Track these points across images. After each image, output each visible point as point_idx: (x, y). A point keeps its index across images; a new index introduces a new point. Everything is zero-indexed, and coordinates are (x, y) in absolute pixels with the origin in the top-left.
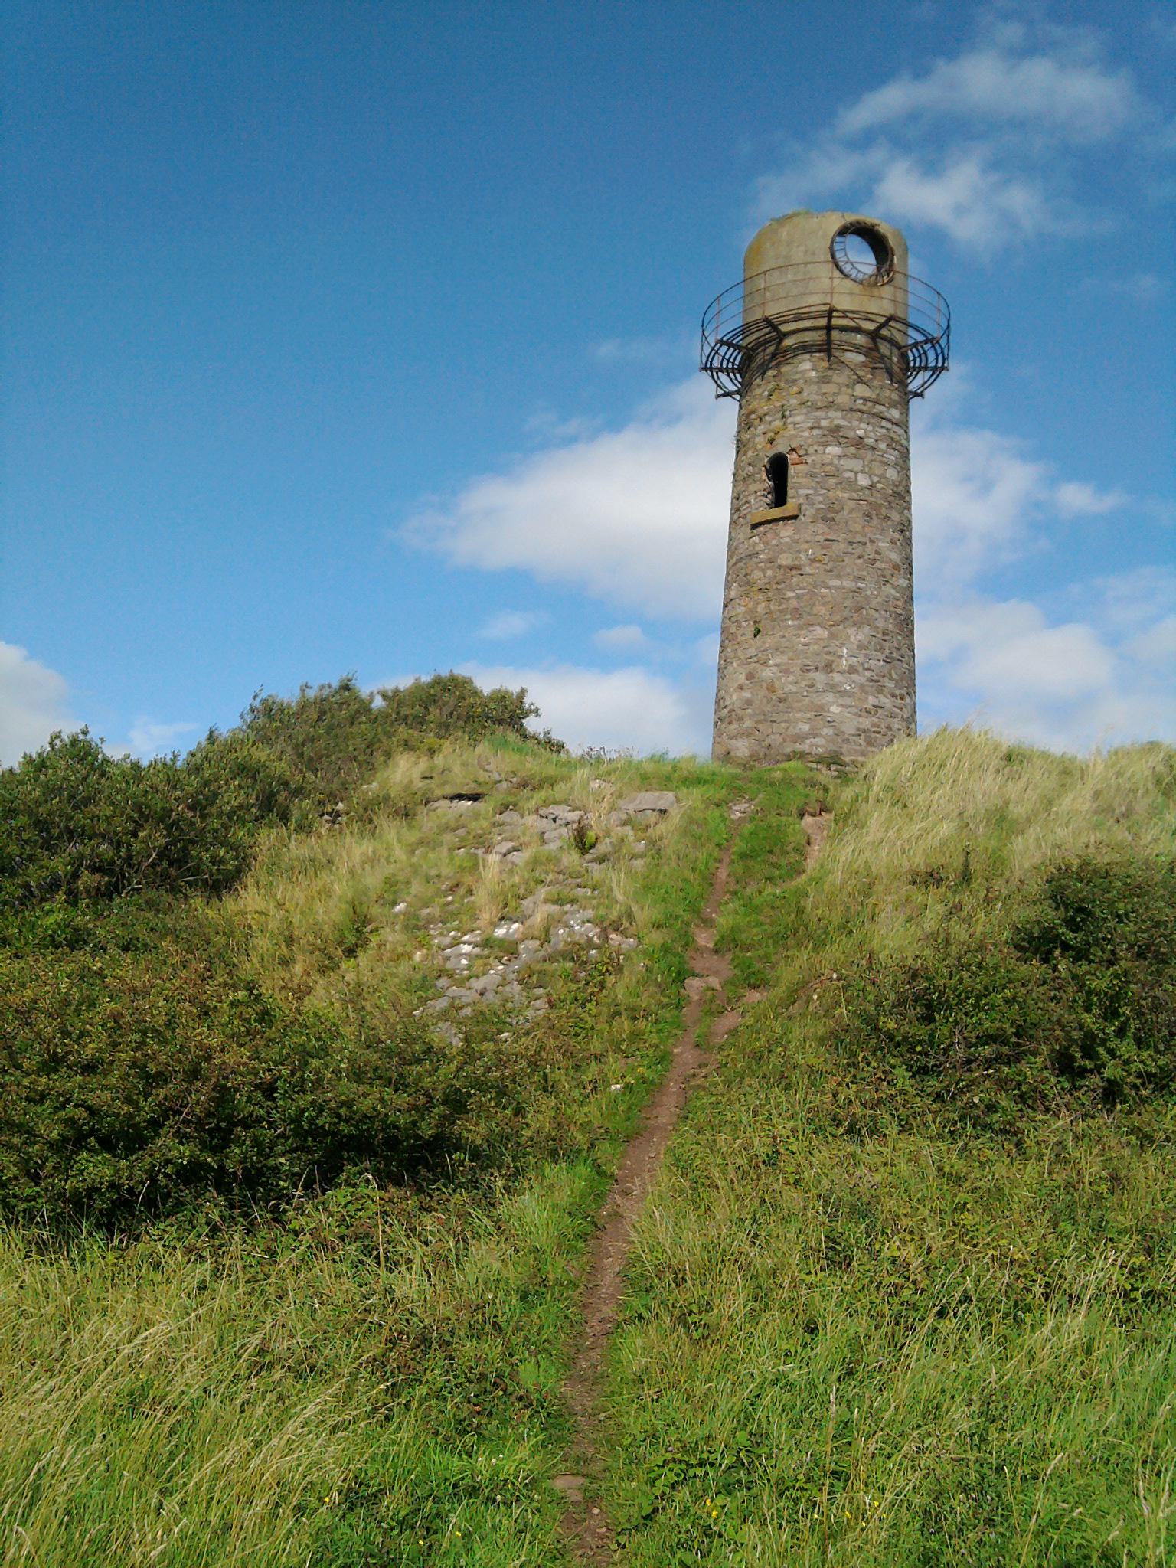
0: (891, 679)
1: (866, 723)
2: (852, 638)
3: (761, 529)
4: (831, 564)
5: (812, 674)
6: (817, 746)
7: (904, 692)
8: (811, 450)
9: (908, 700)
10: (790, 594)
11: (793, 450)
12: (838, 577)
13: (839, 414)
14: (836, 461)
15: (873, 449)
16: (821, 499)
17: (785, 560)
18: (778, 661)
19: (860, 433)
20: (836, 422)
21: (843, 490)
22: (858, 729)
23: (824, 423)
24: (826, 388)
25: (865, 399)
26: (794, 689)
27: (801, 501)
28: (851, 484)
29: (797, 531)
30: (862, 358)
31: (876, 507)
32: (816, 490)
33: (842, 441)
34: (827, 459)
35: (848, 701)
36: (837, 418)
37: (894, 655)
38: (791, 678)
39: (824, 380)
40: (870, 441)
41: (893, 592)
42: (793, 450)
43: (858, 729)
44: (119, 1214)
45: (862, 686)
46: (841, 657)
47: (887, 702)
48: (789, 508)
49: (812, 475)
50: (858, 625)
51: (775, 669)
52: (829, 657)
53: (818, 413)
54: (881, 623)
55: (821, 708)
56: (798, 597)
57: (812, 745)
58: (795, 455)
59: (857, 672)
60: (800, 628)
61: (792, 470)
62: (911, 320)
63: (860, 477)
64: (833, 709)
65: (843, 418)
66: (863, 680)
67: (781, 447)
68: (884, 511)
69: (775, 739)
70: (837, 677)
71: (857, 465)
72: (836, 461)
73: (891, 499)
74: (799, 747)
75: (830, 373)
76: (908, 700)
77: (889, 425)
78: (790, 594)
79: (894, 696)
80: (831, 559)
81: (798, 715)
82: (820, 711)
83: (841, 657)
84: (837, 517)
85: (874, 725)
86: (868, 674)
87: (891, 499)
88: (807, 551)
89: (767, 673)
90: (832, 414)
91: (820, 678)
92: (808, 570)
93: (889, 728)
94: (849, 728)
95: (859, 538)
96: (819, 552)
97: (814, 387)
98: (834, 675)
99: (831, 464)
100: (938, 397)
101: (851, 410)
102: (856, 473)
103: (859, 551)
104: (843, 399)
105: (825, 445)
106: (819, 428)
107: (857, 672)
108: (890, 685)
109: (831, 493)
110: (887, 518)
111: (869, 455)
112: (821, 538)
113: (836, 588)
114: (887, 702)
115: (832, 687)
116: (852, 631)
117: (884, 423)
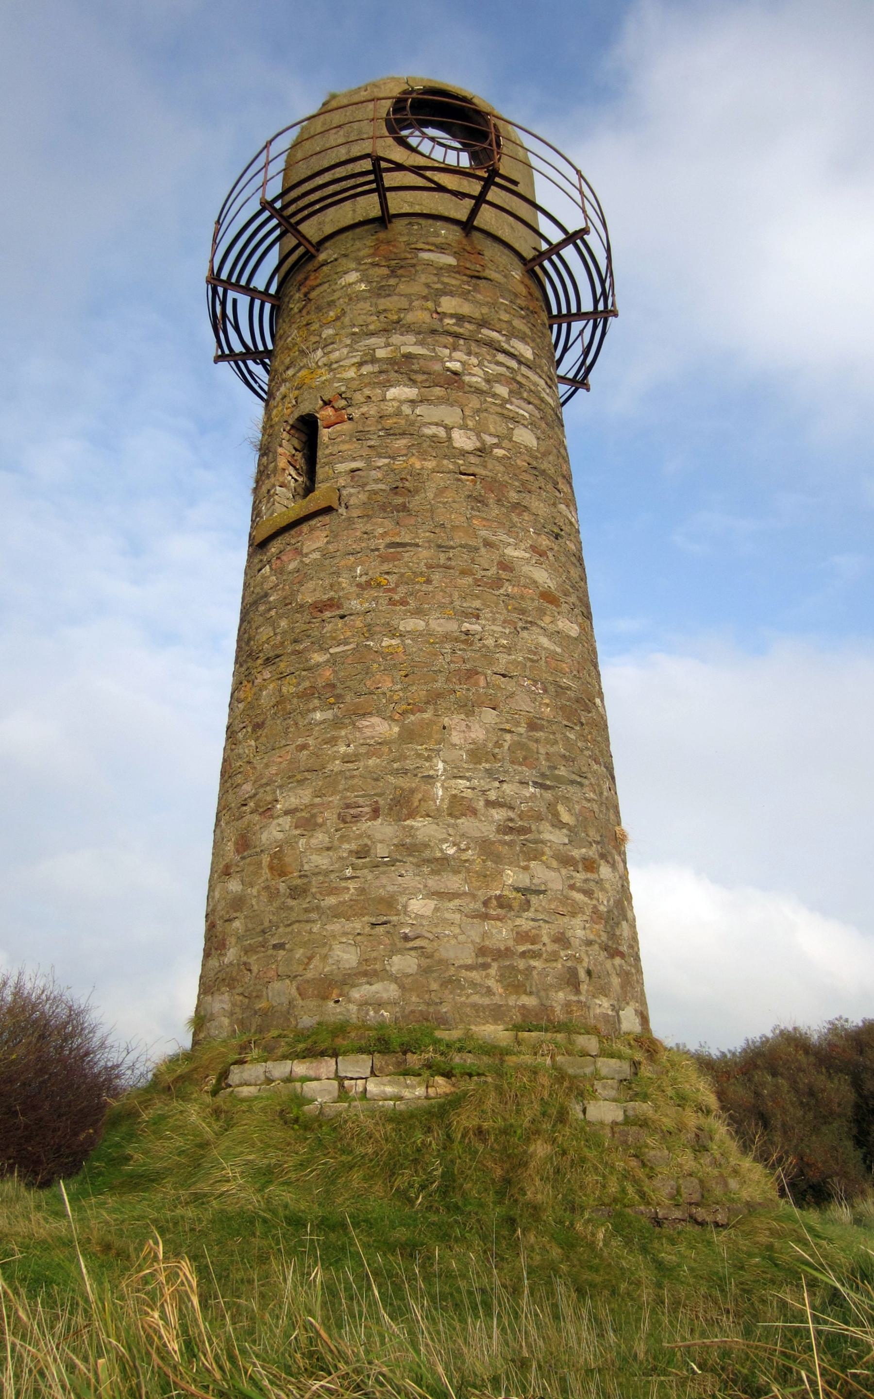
0: (558, 824)
1: (501, 934)
2: (456, 738)
3: (273, 549)
4: (402, 590)
5: (365, 825)
6: (379, 1005)
7: (592, 852)
8: (359, 397)
9: (605, 871)
10: (318, 658)
11: (327, 403)
12: (419, 612)
13: (411, 338)
14: (406, 409)
15: (479, 391)
16: (378, 474)
17: (308, 595)
18: (293, 801)
19: (456, 366)
20: (405, 350)
21: (423, 455)
22: (482, 951)
23: (381, 353)
24: (383, 303)
25: (460, 319)
26: (322, 861)
27: (342, 482)
28: (442, 447)
29: (334, 536)
30: (451, 261)
31: (492, 484)
32: (368, 459)
33: (420, 378)
34: (389, 408)
35: (454, 882)
36: (409, 345)
37: (562, 771)
38: (320, 838)
39: (381, 291)
40: (476, 379)
41: (545, 641)
42: (327, 403)
43: (482, 951)
44: (304, 1058)
45: (485, 846)
46: (430, 779)
47: (549, 876)
48: (320, 497)
49: (360, 436)
50: (468, 708)
51: (286, 822)
52: (404, 783)
53: (373, 341)
54: (524, 704)
55: (389, 903)
56: (334, 660)
57: (364, 1004)
58: (329, 411)
59: (474, 812)
60: (337, 723)
61: (324, 434)
62: (539, 201)
63: (456, 434)
64: (419, 906)
65: (421, 343)
66: (488, 831)
67: (305, 408)
68: (513, 496)
69: (280, 992)
70: (423, 828)
71: (451, 415)
72: (406, 409)
73: (525, 476)
74: (333, 1012)
75: (392, 281)
76: (605, 871)
77: (514, 364)
78: (318, 658)
79: (566, 861)
80: (402, 580)
81: (335, 927)
82: (382, 910)
83: (430, 779)
84: (414, 503)
85: (523, 937)
86: (499, 815)
87: (525, 476)
88: (352, 569)
89: (273, 833)
90: (396, 339)
91: (383, 832)
92: (355, 604)
93: (562, 940)
94: (458, 950)
95: (460, 538)
96: (376, 569)
97: (366, 306)
98: (417, 823)
99: (398, 413)
100: (581, 174)
101: (434, 332)
102: (448, 429)
103: (462, 560)
104: (420, 316)
105: (388, 385)
106: (374, 360)
107: (474, 812)
108: (556, 837)
109: (399, 463)
110: (519, 507)
111: (474, 402)
112: (381, 543)
113: (416, 635)
114: (549, 876)
115: (410, 849)
116: (454, 720)
117: (501, 357)
